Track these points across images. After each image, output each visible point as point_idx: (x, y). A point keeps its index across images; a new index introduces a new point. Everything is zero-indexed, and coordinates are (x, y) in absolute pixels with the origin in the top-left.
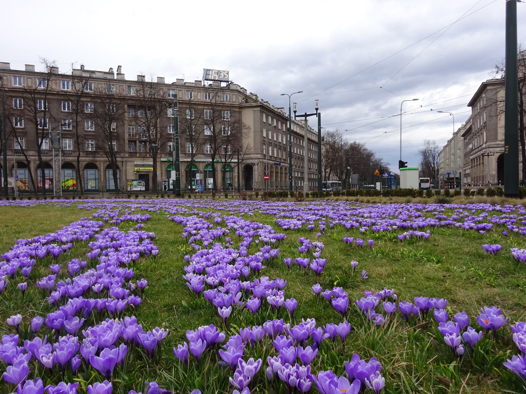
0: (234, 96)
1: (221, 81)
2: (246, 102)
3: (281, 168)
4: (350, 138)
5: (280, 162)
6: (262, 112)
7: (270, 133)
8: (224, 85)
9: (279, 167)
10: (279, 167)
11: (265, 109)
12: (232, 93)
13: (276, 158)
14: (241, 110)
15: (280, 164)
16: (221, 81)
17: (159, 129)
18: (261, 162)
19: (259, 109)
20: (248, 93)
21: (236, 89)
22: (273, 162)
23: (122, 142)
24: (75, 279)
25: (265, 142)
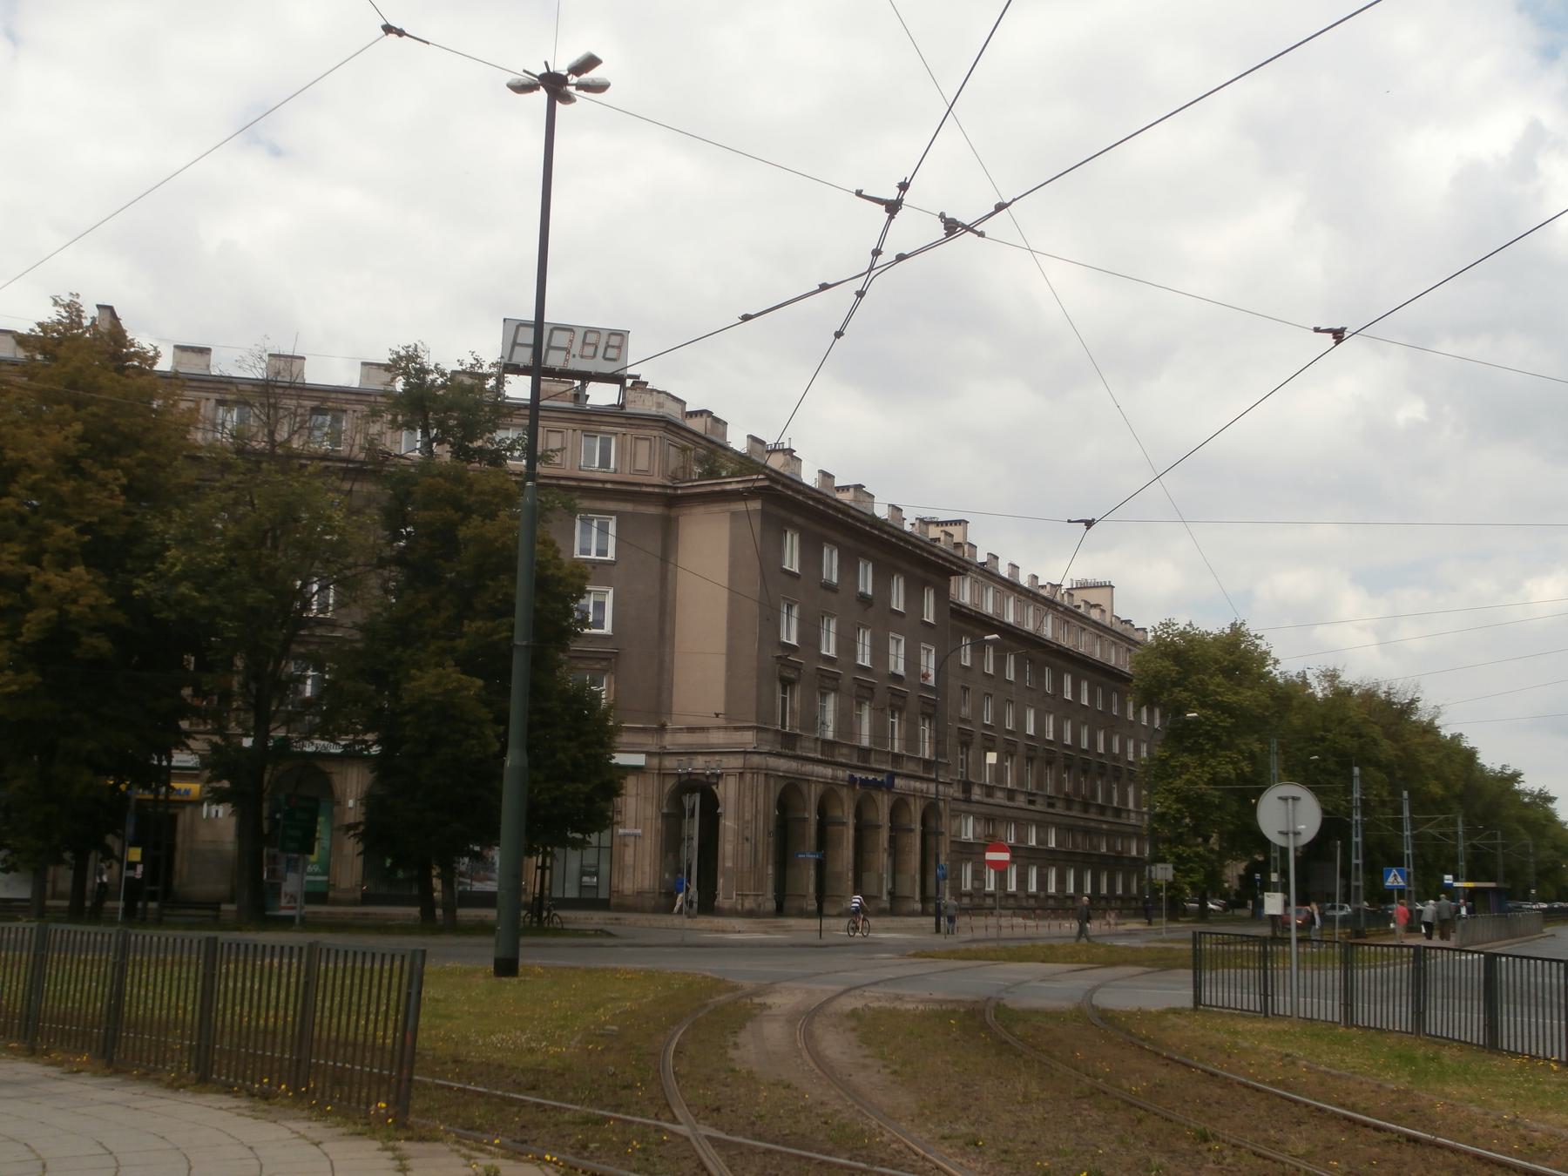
0: (643, 447)
1: (587, 377)
2: (712, 473)
3: (899, 805)
4: (1157, 587)
5: (892, 776)
6: (774, 526)
7: (1068, 727)
8: (602, 395)
9: (883, 804)
10: (884, 802)
11: (787, 504)
12: (632, 431)
13: (864, 753)
14: (673, 512)
15: (889, 786)
16: (587, 377)
17: (1357, 839)
18: (756, 770)
19: (756, 505)
20: (737, 441)
21: (653, 411)
22: (842, 774)
23: (253, 686)
24: (1093, 927)
25: (789, 671)
